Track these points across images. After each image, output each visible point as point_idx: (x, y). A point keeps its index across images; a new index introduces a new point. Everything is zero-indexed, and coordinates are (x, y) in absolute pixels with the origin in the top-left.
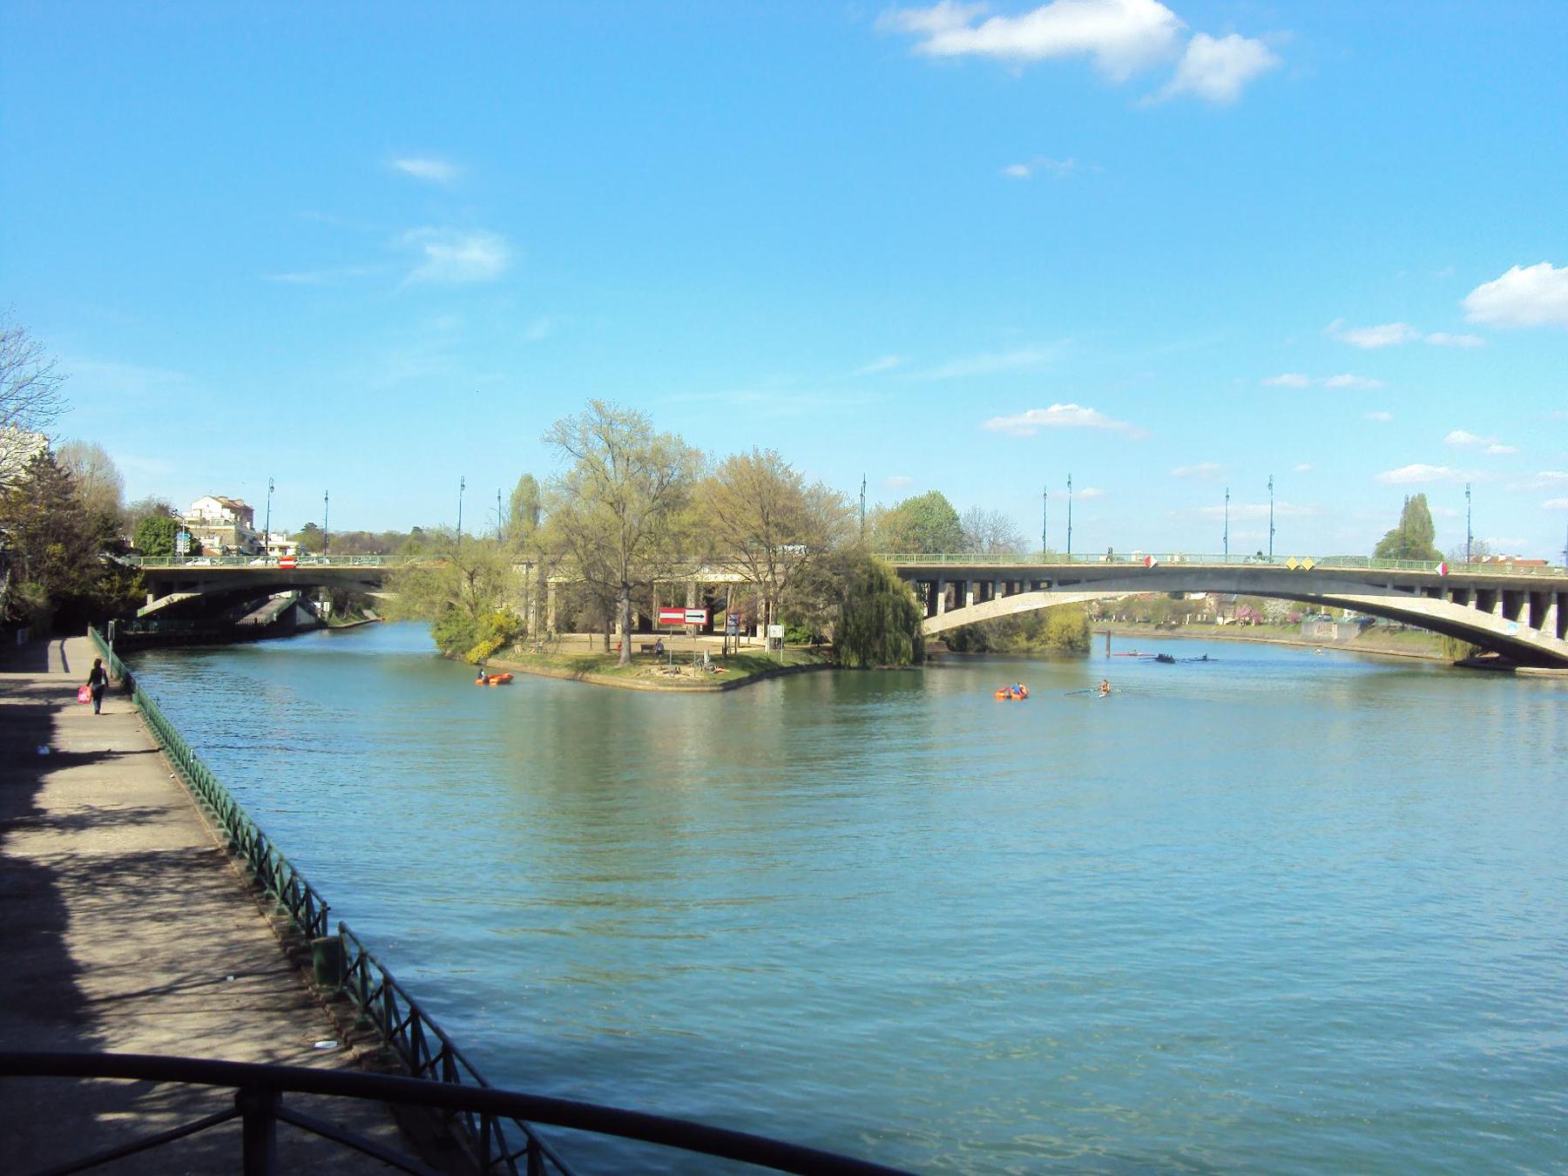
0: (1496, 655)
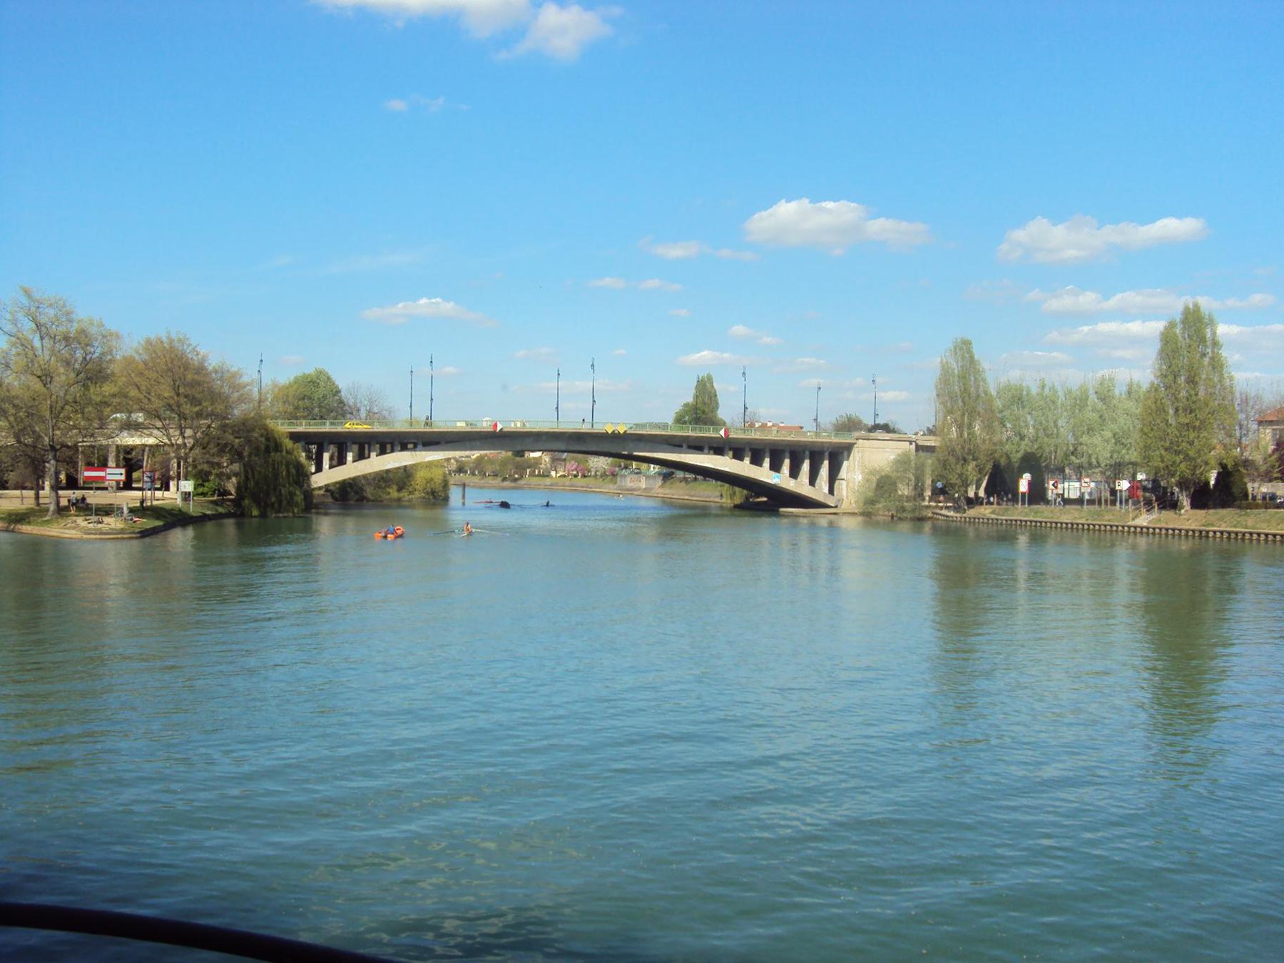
0: (765, 499)
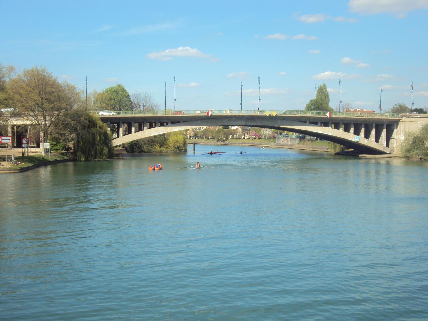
0: (352, 150)
